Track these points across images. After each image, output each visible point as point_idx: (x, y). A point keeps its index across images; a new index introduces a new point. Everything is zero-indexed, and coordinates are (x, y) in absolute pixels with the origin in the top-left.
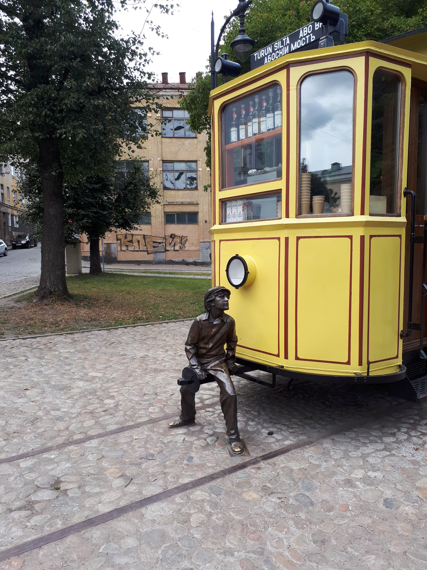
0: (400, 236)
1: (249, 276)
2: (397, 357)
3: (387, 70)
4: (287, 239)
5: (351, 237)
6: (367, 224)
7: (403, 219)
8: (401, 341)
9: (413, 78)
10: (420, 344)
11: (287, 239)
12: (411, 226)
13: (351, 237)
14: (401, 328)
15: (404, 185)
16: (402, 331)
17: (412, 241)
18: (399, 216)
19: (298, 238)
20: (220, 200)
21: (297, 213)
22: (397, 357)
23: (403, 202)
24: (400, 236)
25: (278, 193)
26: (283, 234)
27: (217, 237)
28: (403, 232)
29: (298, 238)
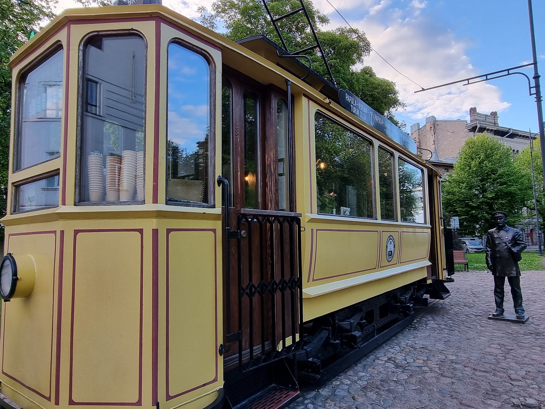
0: (214, 231)
1: (19, 283)
2: (215, 380)
3: (189, 45)
4: (62, 232)
5: (141, 231)
6: (160, 215)
7: (218, 210)
8: (221, 359)
9: (224, 65)
10: (239, 360)
11: (62, 232)
12: (226, 217)
13: (141, 231)
14: (221, 341)
15: (219, 172)
16: (221, 345)
17: (229, 237)
18: (214, 206)
19: (76, 232)
20: (13, 183)
21: (77, 198)
22: (215, 380)
23: (219, 190)
24: (214, 231)
25: (56, 173)
26: (58, 226)
27: (8, 231)
28: (218, 225)
29: (76, 232)
